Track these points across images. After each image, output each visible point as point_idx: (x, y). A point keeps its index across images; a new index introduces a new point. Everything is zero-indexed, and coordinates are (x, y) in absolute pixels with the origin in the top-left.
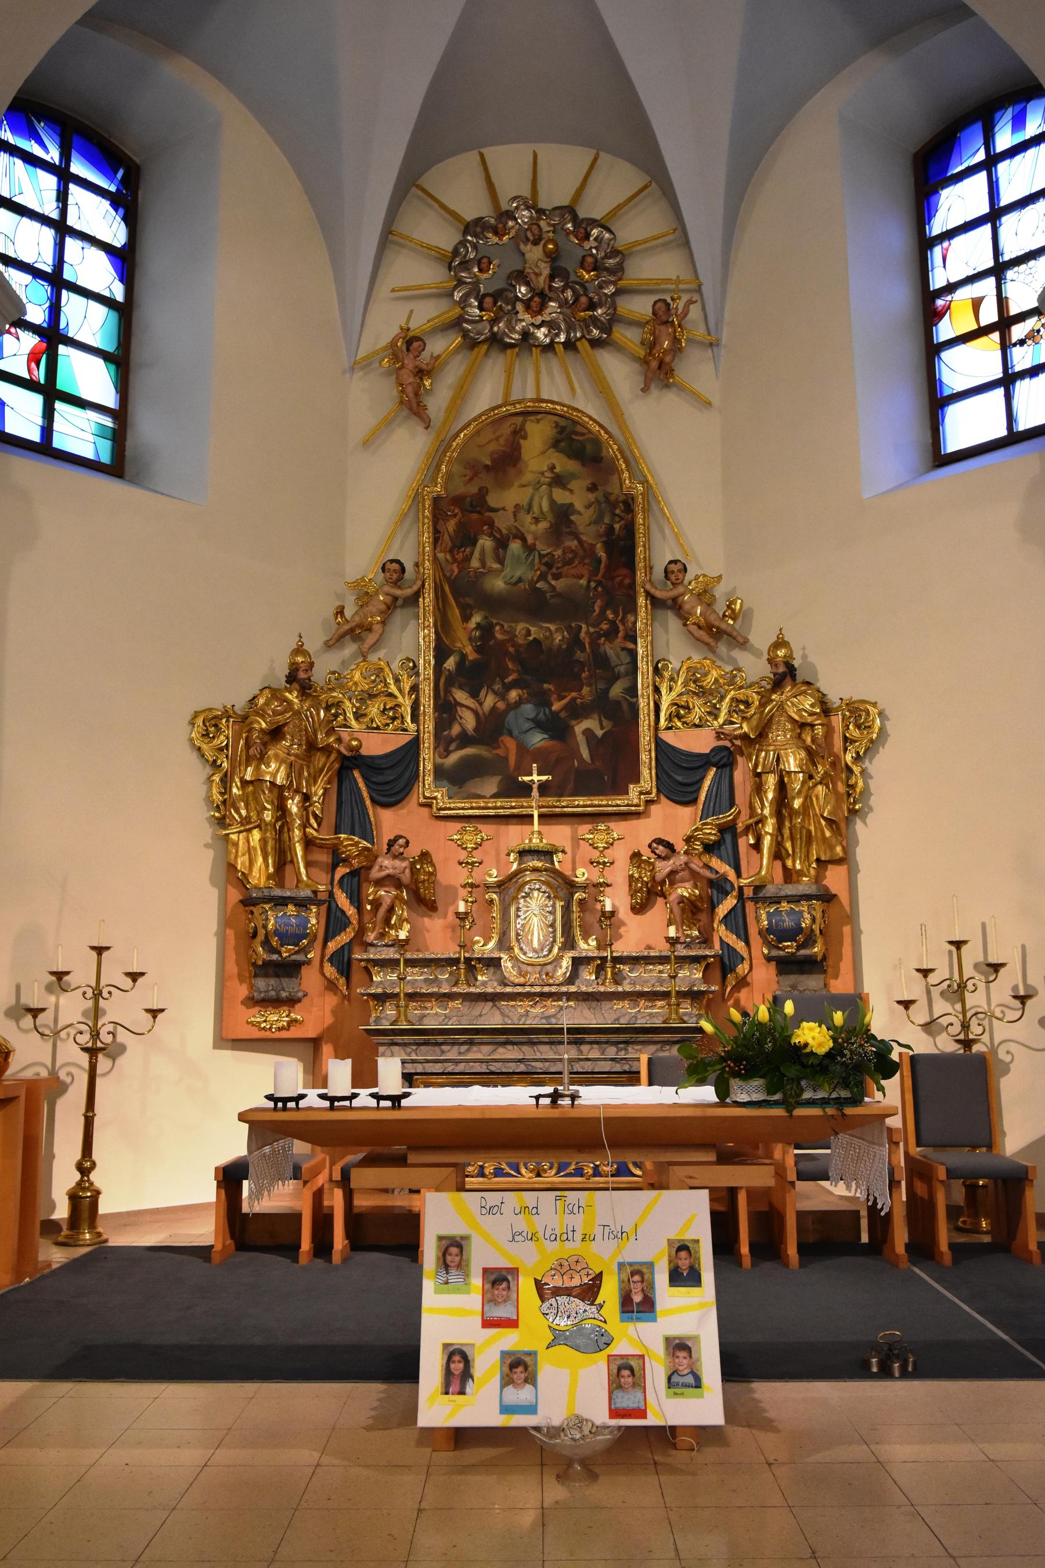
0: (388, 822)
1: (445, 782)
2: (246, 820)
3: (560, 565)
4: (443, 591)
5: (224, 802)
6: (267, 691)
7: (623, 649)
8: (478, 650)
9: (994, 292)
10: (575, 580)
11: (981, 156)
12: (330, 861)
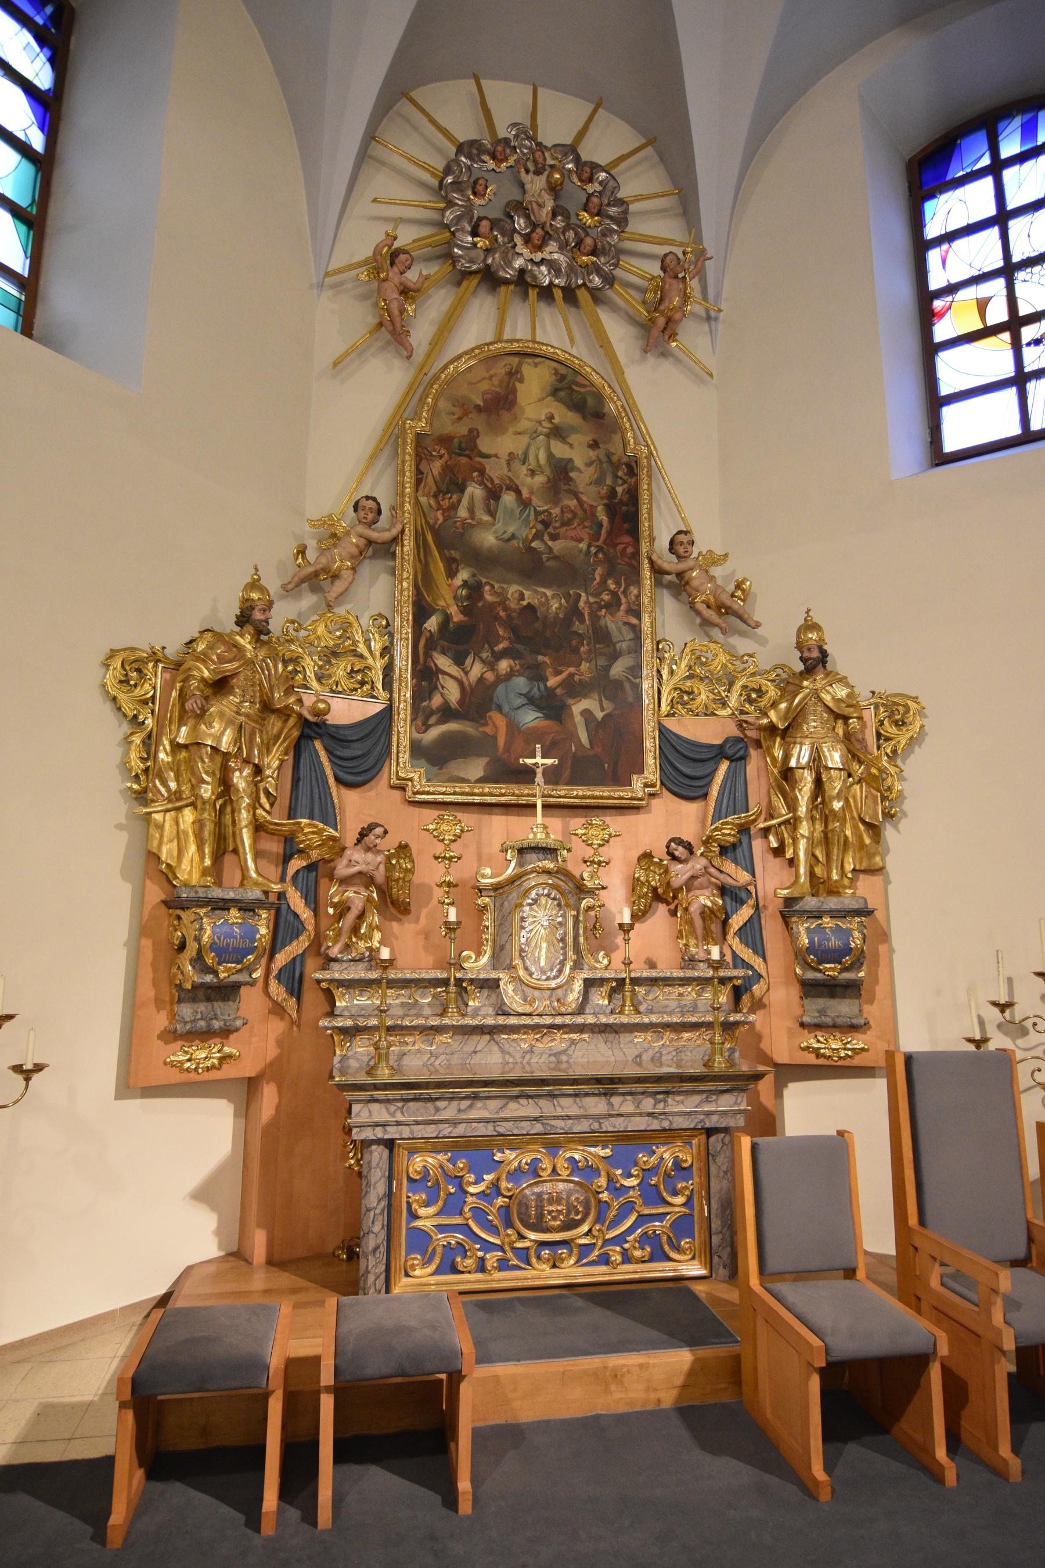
0: (355, 807)
1: (423, 762)
2: (177, 795)
3: (557, 525)
4: (425, 540)
5: (146, 771)
6: (208, 636)
7: (626, 623)
8: (464, 611)
9: (1004, 292)
10: (575, 543)
11: (986, 161)
12: (281, 851)
